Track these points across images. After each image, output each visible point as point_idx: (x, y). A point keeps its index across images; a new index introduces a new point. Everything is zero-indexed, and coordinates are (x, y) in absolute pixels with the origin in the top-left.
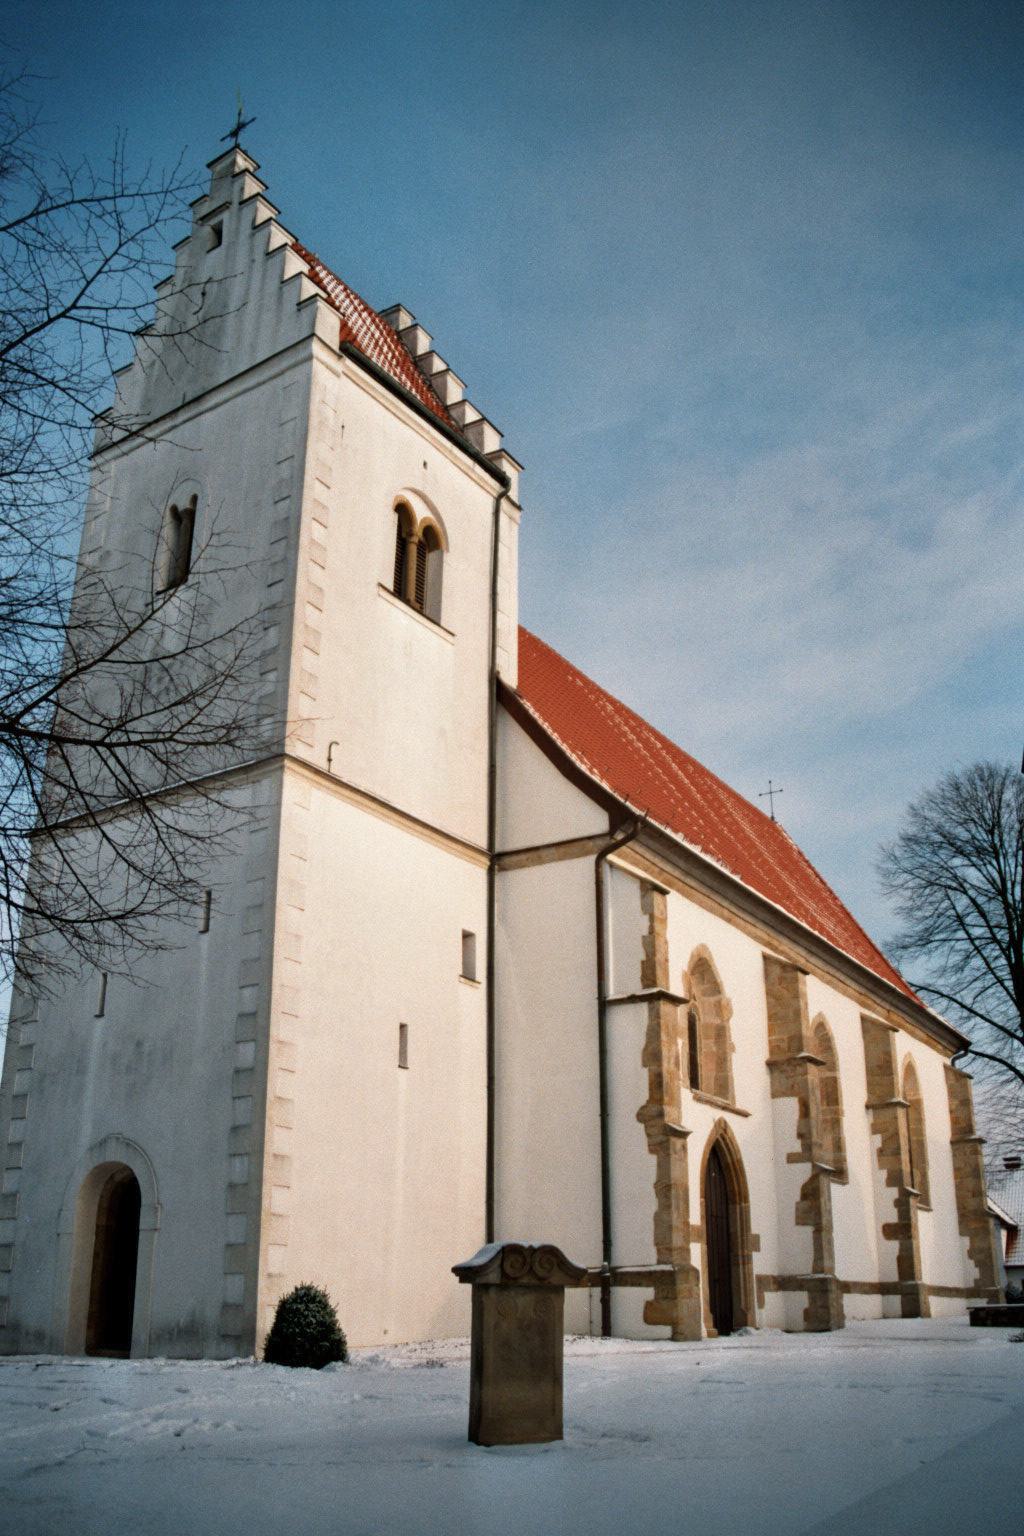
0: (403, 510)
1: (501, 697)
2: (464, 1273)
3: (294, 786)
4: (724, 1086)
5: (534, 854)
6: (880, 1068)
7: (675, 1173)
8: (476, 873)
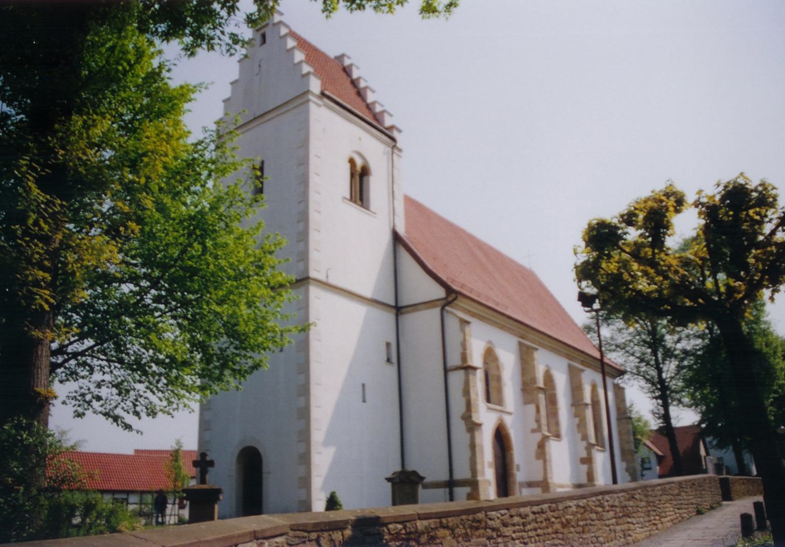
0: (352, 162)
1: (397, 238)
2: (388, 480)
3: (314, 292)
4: (500, 402)
5: (415, 307)
6: (576, 389)
7: (477, 441)
8: (390, 317)
